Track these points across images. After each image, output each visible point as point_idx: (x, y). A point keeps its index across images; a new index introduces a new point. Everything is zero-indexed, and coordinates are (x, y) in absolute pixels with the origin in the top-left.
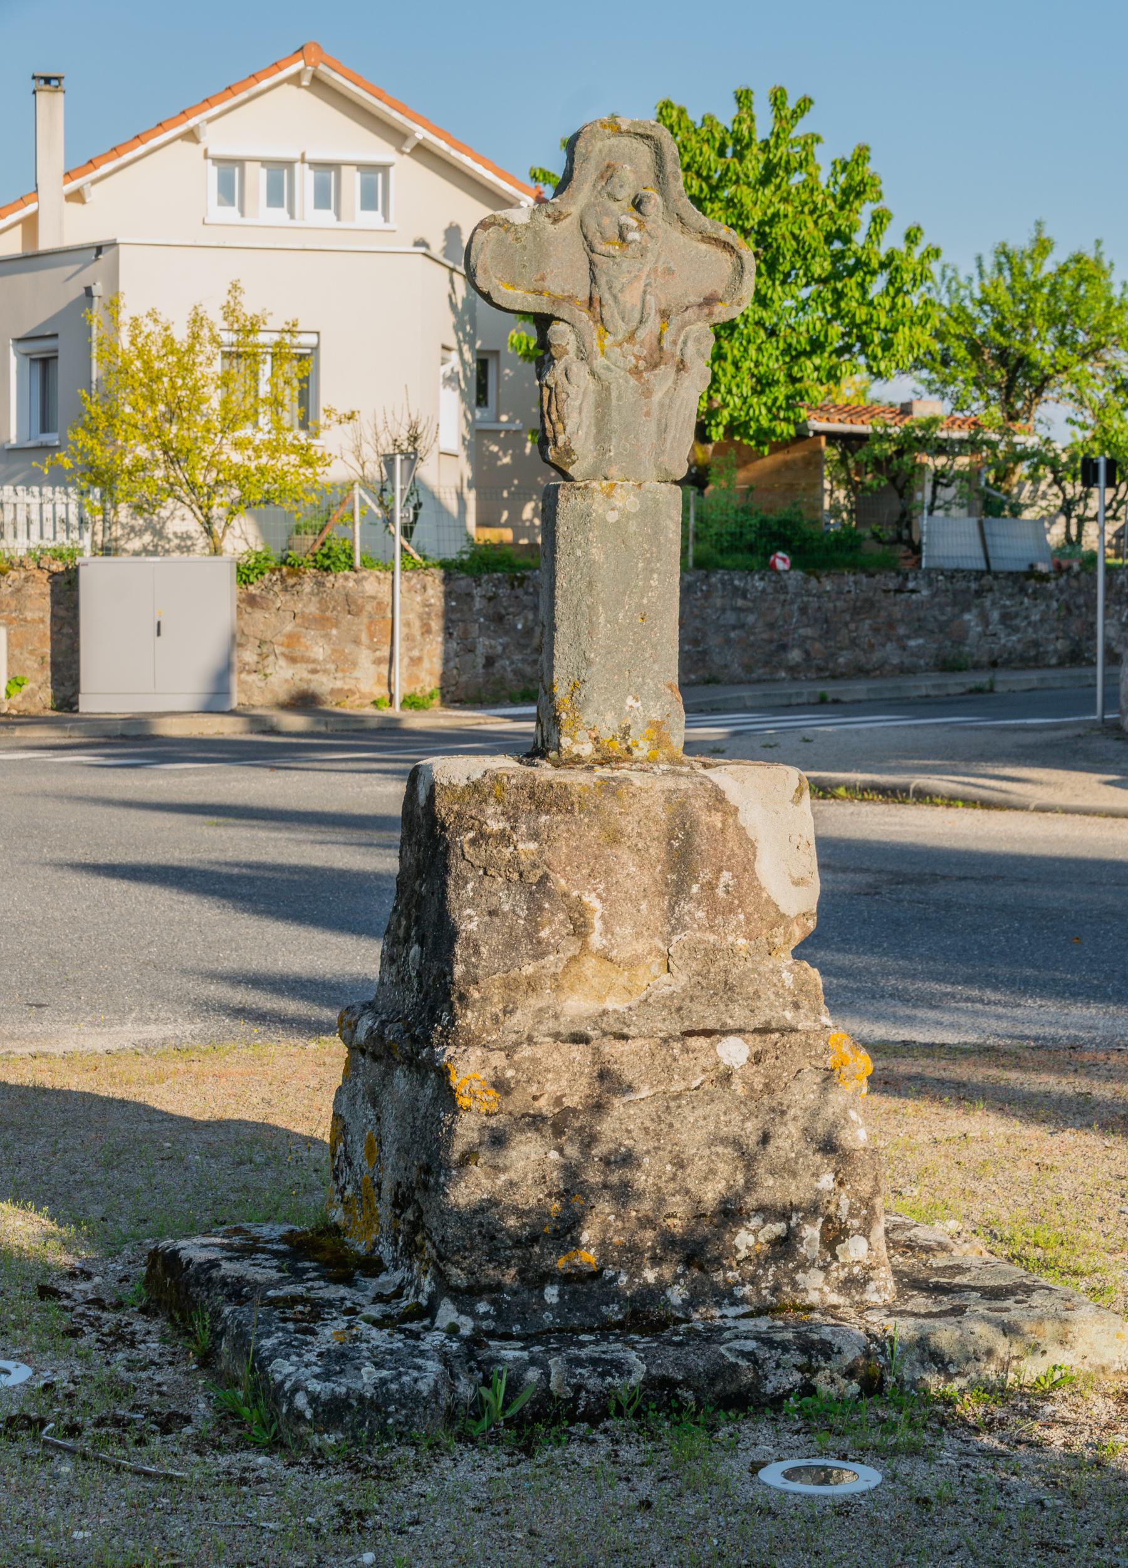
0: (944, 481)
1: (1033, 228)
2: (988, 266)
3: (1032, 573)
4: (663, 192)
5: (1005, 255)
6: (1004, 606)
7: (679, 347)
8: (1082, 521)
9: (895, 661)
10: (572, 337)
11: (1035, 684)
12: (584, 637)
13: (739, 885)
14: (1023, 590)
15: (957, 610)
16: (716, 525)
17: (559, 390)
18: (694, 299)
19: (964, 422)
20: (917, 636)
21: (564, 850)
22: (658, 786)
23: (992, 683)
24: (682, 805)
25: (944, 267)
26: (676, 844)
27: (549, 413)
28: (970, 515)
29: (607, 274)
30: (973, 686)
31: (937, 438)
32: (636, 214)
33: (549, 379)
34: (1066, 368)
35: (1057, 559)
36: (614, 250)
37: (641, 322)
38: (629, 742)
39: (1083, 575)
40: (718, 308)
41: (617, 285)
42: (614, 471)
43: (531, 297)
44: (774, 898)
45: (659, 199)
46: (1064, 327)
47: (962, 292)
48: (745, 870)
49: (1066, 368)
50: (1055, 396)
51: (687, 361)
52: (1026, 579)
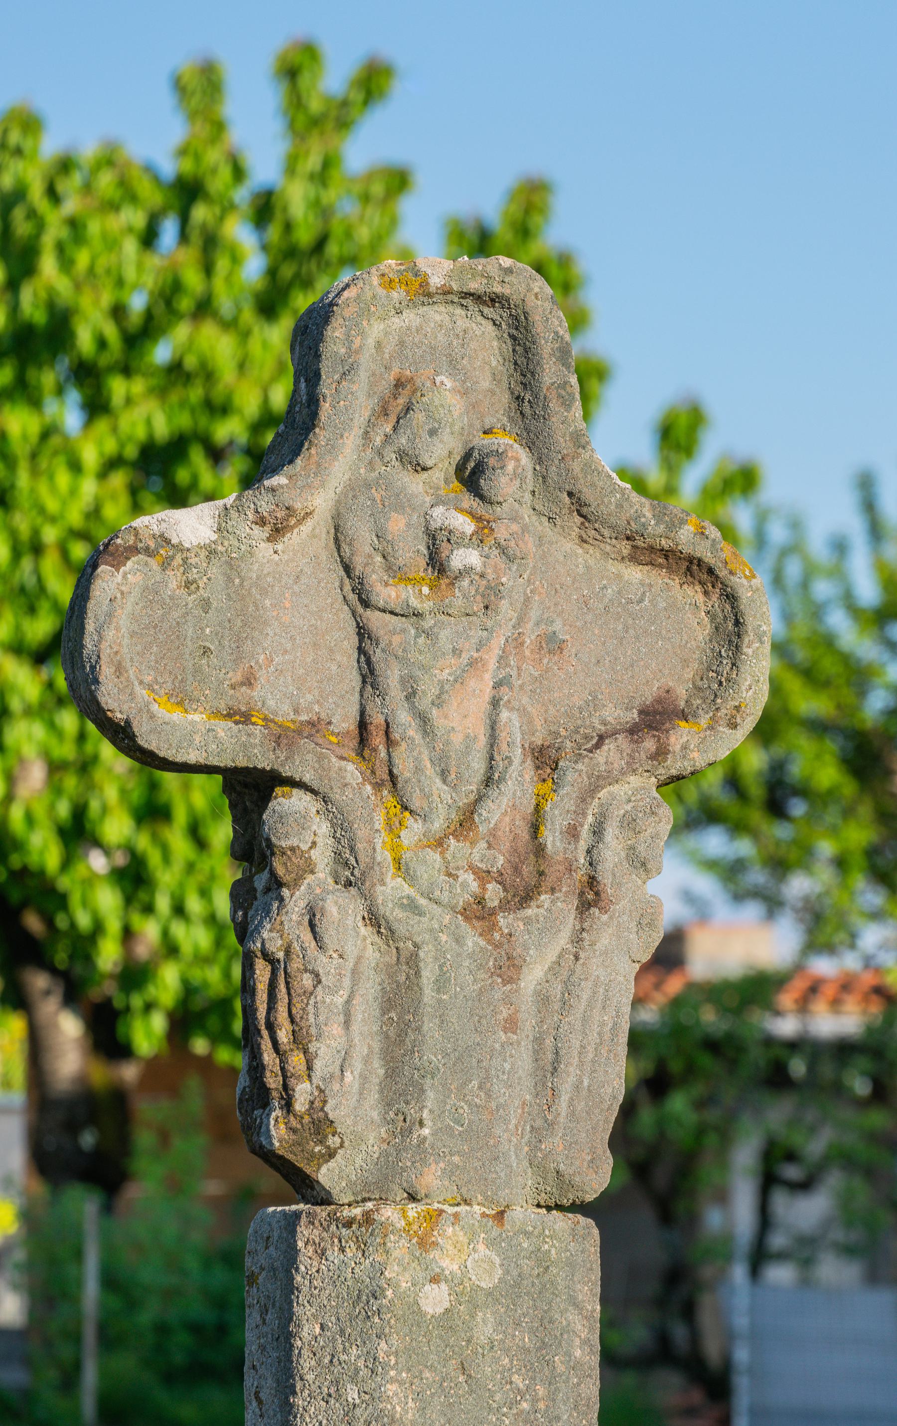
7: (583, 845)
10: (323, 828)
17: (295, 965)
18: (616, 714)
27: (271, 1027)
29: (402, 660)
32: (468, 501)
33: (270, 938)
36: (416, 596)
37: (488, 781)
40: (681, 736)
41: (428, 689)
42: (431, 1178)
43: (224, 729)
45: (524, 457)
51: (606, 879)
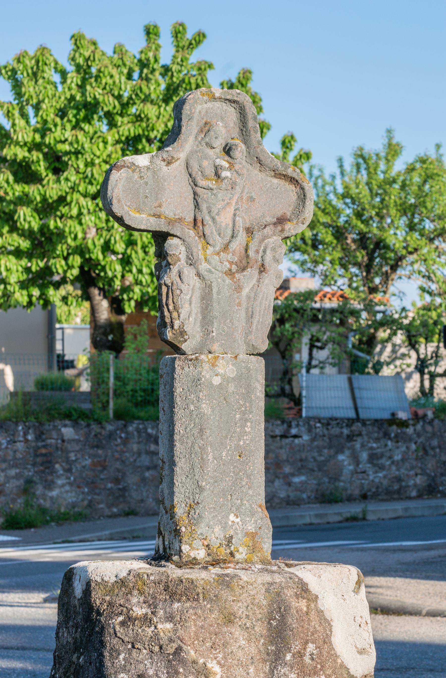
0: (319, 344)
1: (385, 134)
2: (348, 166)
3: (393, 420)
4: (246, 142)
5: (362, 158)
6: (372, 448)
7: (260, 255)
8: (433, 377)
9: (282, 495)
10: (183, 249)
11: (400, 513)
12: (197, 470)
13: (320, 654)
14: (386, 435)
15: (332, 452)
16: (132, 383)
17: (174, 287)
18: (270, 219)
19: (333, 295)
20: (300, 474)
21: (193, 629)
22: (259, 581)
23: (364, 512)
24: (278, 594)
25: (311, 168)
26: (274, 623)
27: (167, 305)
28: (340, 372)
30: (348, 515)
31: (312, 309)
32: (227, 158)
33: (167, 279)
34: (416, 250)
35: (414, 409)
36: (211, 184)
37: (233, 237)
38: (232, 548)
39: (436, 422)
41: (215, 211)
42: (216, 347)
43: (152, 219)
44: (346, 663)
46: (413, 215)
47: (328, 188)
48: (325, 642)
49: (416, 250)
50: (408, 273)
52: (389, 425)
